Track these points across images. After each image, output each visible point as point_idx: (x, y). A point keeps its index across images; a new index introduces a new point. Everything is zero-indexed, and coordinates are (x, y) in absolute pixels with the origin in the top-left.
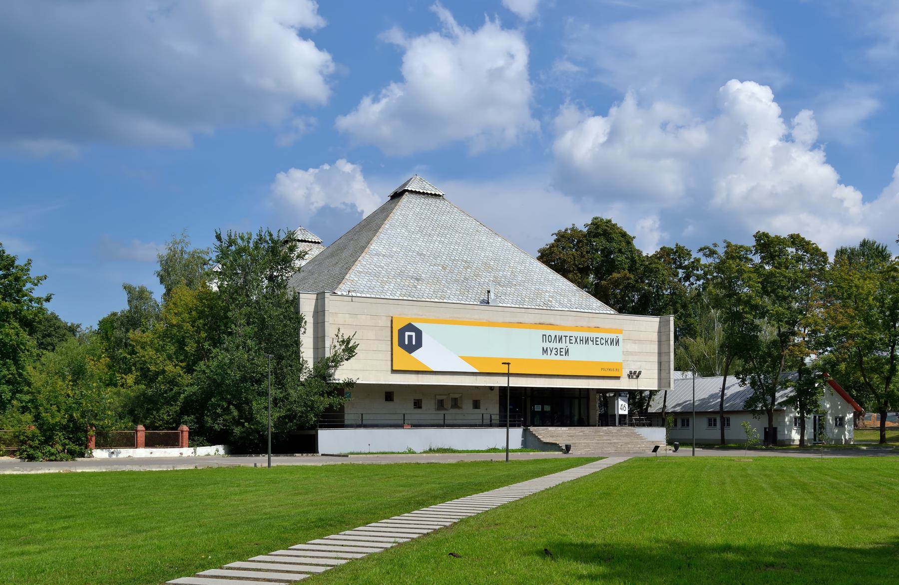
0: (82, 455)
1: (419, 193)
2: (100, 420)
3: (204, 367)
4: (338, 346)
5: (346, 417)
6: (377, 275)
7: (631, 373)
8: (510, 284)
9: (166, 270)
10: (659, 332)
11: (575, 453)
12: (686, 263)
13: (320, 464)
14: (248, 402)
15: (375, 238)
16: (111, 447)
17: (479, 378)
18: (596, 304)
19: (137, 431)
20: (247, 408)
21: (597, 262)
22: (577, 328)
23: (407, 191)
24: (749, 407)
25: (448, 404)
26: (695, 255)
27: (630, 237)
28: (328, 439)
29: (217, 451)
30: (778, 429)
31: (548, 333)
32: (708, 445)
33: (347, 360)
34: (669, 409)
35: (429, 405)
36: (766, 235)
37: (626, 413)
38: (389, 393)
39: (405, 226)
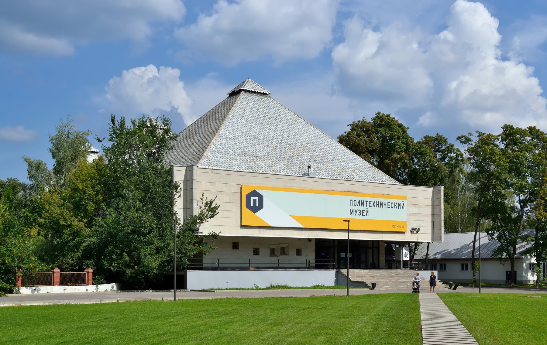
0: (11, 292)
1: (252, 92)
2: (26, 264)
3: (101, 223)
4: (203, 207)
5: (204, 261)
6: (227, 153)
7: (413, 229)
8: (322, 162)
9: (56, 148)
10: (433, 199)
11: (379, 289)
12: (444, 148)
13: (211, 298)
14: (136, 249)
15: (223, 125)
16: (33, 284)
17: (304, 232)
18: (384, 177)
19: (54, 272)
20: (136, 254)
21: (382, 145)
22: (374, 195)
23: (243, 90)
24: (496, 256)
25: (278, 252)
26: (449, 142)
27: (405, 128)
28: (193, 278)
29: (113, 287)
30: (517, 273)
31: (353, 198)
32: (465, 284)
33: (210, 218)
34: (431, 256)
35: (264, 252)
36: (511, 127)
37: (408, 259)
38: (235, 243)
39: (243, 117)
